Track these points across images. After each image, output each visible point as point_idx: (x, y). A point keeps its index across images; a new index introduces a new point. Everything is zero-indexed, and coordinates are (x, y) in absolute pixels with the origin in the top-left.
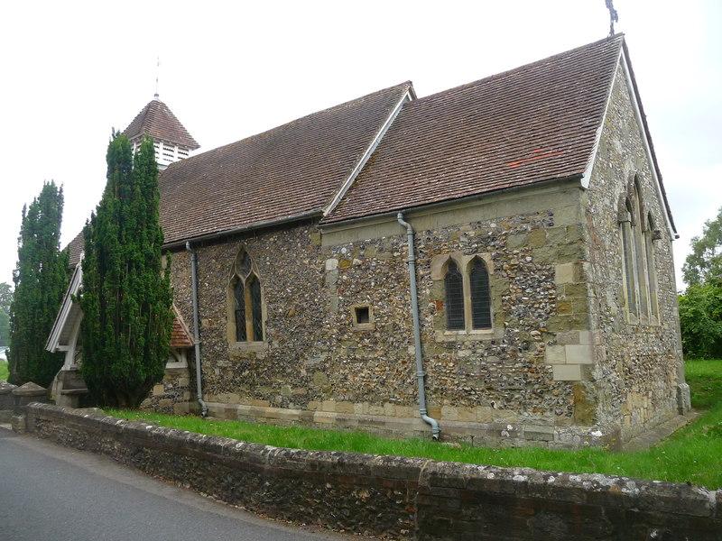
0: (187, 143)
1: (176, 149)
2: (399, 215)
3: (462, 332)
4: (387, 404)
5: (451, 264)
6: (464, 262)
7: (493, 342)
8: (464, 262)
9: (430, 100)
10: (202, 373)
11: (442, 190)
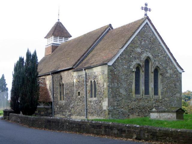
0: (68, 36)
1: (63, 38)
3: (92, 98)
5: (91, 81)
6: (93, 81)
8: (93, 81)
9: (116, 29)
11: (55, 80)
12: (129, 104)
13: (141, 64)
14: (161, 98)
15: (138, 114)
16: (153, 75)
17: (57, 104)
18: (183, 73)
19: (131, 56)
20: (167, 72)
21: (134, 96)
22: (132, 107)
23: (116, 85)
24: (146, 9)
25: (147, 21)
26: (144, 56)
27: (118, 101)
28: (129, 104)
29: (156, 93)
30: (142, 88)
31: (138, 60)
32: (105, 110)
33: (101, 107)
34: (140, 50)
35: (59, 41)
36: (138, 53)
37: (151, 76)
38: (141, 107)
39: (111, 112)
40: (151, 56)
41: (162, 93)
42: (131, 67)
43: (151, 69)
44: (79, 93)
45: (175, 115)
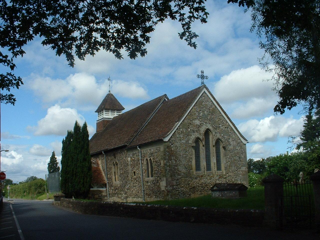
2: (138, 147)
4: (139, 198)
5: (147, 160)
6: (149, 159)
7: (153, 181)
8: (149, 159)
10: (109, 191)
12: (190, 182)
13: (201, 137)
14: (224, 173)
15: (200, 193)
16: (214, 148)
17: (111, 186)
18: (247, 145)
19: (189, 130)
20: (230, 145)
21: (194, 173)
22: (193, 186)
23: (174, 163)
24: (203, 77)
25: (205, 90)
26: (203, 129)
27: (177, 180)
28: (190, 182)
29: (219, 168)
30: (203, 163)
31: (197, 134)
32: (163, 191)
33: (159, 187)
34: (199, 122)
35: (110, 115)
36: (197, 125)
37: (213, 150)
38: (204, 185)
39: (170, 192)
40: (211, 128)
41: (226, 168)
42: (190, 142)
43: (212, 142)
44: (135, 172)
45: (237, 193)
